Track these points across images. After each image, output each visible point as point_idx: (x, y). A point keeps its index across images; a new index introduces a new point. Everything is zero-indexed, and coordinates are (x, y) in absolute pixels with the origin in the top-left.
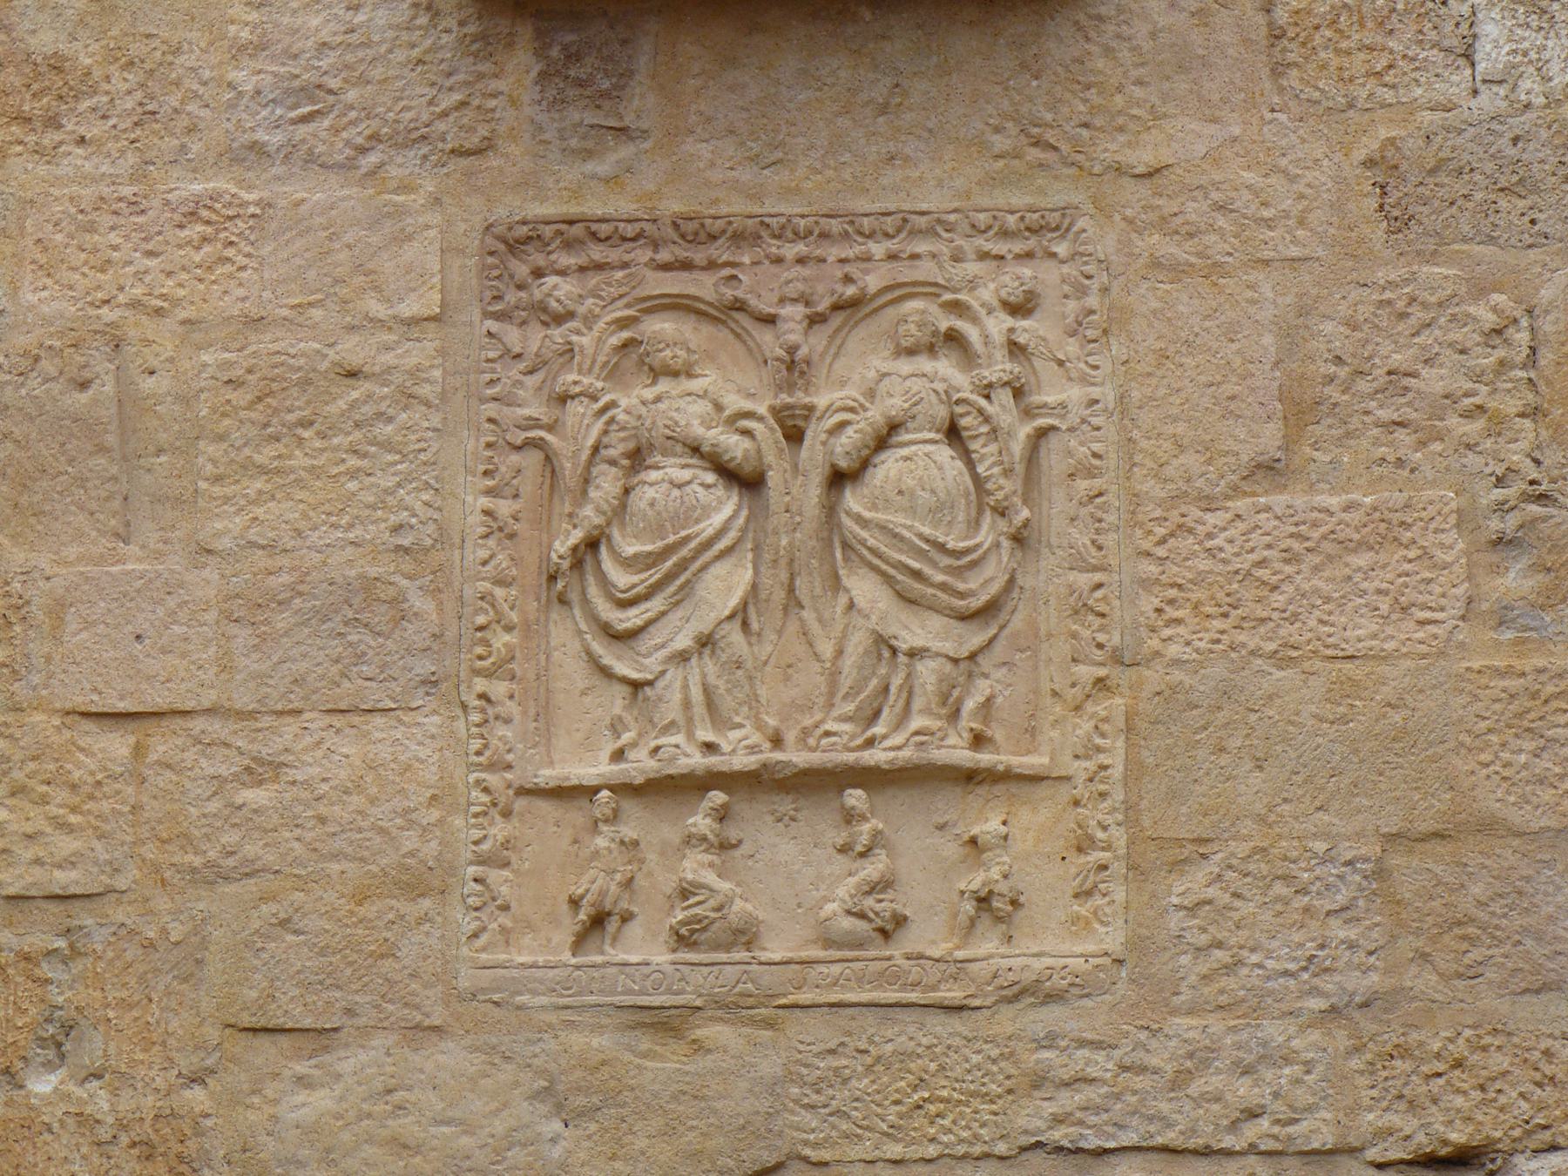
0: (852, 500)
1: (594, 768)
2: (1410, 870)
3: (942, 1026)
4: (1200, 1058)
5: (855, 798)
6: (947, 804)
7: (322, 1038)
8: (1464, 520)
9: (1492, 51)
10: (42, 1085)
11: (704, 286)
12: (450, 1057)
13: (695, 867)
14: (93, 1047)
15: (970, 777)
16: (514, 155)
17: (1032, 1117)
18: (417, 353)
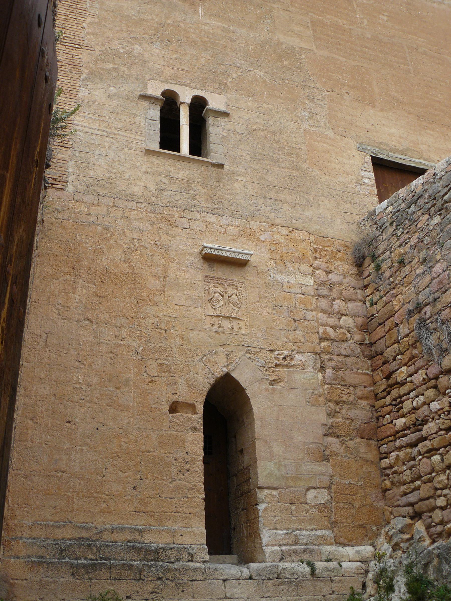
0: (229, 298)
1: (212, 314)
2: (268, 330)
3: (237, 336)
4: (254, 341)
5: (231, 319)
6: (237, 321)
7: (193, 330)
8: (271, 307)
9: (272, 276)
10: (172, 331)
11: (219, 282)
12: (202, 333)
13: (220, 322)
14: (176, 328)
15: (238, 319)
16: (206, 271)
17: (243, 343)
18: (199, 283)
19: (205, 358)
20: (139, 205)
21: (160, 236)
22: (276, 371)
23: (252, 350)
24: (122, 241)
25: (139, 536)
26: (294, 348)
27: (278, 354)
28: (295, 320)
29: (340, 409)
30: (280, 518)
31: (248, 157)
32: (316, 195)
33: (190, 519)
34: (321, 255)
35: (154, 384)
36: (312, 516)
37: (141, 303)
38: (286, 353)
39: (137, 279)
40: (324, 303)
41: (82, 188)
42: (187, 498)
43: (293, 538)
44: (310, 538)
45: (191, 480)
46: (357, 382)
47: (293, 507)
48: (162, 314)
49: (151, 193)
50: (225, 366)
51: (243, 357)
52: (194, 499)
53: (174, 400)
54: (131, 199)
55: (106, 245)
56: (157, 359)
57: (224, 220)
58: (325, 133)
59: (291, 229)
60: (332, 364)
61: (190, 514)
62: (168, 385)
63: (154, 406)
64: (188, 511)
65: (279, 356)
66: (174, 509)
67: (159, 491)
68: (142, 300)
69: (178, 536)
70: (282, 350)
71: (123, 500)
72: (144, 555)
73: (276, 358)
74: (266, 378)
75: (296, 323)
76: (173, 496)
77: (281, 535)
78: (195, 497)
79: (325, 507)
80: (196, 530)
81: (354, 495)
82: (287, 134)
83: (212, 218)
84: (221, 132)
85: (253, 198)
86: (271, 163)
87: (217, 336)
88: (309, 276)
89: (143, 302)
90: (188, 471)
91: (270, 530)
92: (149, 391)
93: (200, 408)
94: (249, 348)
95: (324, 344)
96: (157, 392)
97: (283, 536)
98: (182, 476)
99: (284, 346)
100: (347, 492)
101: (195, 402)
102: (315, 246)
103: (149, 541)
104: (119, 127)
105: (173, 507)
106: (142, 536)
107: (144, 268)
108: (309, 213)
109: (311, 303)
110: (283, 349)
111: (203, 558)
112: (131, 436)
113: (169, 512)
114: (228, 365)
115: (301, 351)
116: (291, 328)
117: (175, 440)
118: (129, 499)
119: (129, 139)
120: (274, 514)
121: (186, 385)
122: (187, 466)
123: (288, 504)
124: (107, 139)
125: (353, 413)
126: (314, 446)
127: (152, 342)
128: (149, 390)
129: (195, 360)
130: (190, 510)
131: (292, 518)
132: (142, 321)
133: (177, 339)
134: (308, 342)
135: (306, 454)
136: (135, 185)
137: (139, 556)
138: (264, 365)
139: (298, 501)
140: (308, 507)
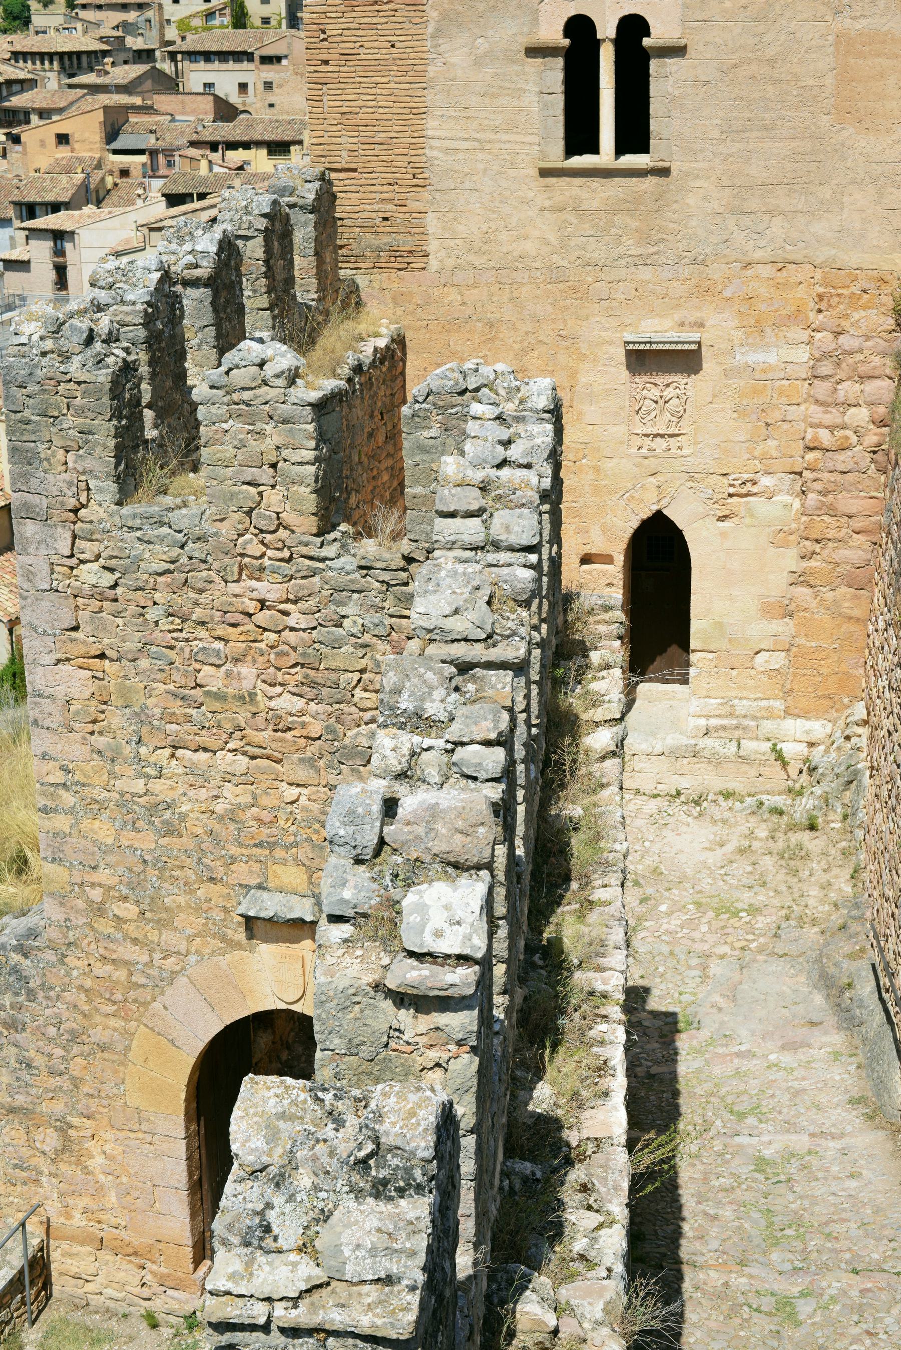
12: (624, 460)
17: (683, 468)
20: (533, 273)
21: (565, 321)
23: (696, 475)
24: (511, 340)
26: (759, 467)
28: (767, 424)
29: (822, 548)
31: (716, 134)
32: (839, 185)
34: (830, 306)
38: (746, 476)
40: (822, 389)
41: (450, 262)
46: (854, 511)
47: (734, 673)
49: (550, 248)
54: (520, 266)
55: (489, 350)
57: (666, 273)
58: (885, 28)
59: (781, 265)
60: (818, 486)
79: (779, 673)
81: (823, 659)
82: (799, 56)
83: (646, 274)
84: (670, 89)
85: (719, 220)
86: (759, 134)
88: (803, 345)
93: (620, 559)
95: (811, 456)
100: (813, 657)
102: (821, 290)
104: (497, 123)
108: (819, 228)
109: (798, 392)
114: (659, 501)
119: (513, 146)
124: (480, 155)
125: (844, 553)
126: (773, 599)
134: (784, 456)
136: (525, 237)
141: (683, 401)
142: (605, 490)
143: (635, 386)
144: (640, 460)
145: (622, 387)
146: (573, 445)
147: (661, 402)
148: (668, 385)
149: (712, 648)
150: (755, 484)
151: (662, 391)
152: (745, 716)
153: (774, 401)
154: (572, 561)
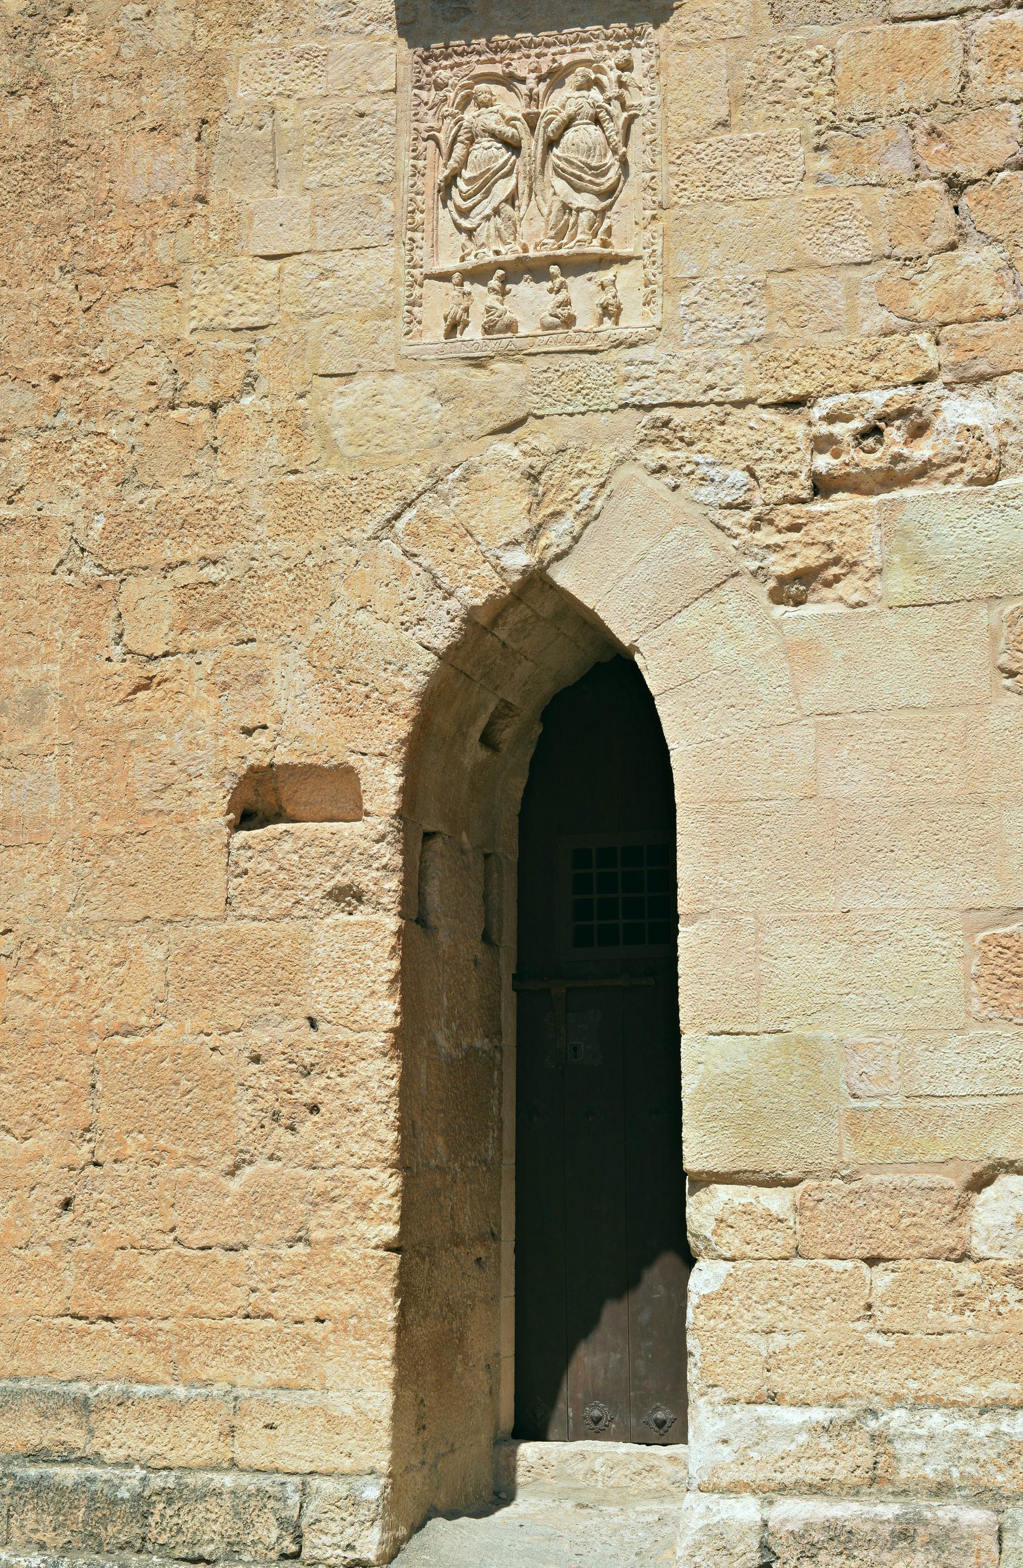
12: (396, 381)
14: (262, 387)
17: (623, 393)
19: (410, 514)
22: (812, 518)
23: (679, 416)
25: (80, 1433)
26: (933, 357)
27: (831, 418)
28: (956, 185)
30: (799, 1338)
33: (318, 1347)
35: (159, 694)
36: (999, 1324)
37: (94, 289)
38: (878, 399)
39: (69, 167)
42: (308, 1242)
43: (862, 1453)
44: (967, 1454)
45: (327, 1154)
47: (882, 1278)
48: (193, 324)
50: (516, 543)
51: (626, 471)
52: (338, 1248)
53: (251, 761)
56: (170, 567)
61: (320, 1320)
62: (225, 686)
63: (158, 804)
64: (307, 1309)
65: (839, 429)
66: (239, 1297)
67: (174, 1217)
68: (99, 272)
69: (251, 1430)
70: (855, 389)
71: (18, 1264)
72: (85, 1523)
73: (822, 444)
74: (754, 565)
75: (964, 201)
76: (242, 1237)
77: (789, 1433)
78: (343, 1238)
80: (341, 1404)
87: (481, 376)
89: (102, 281)
90: (314, 1109)
91: (734, 1401)
92: (132, 735)
94: (662, 413)
96: (170, 735)
97: (803, 1438)
98: (288, 1137)
99: (873, 358)
101: (353, 760)
103: (122, 1453)
105: (240, 1292)
106: (90, 1431)
107: (103, 99)
110: (862, 380)
111: (350, 1547)
112: (54, 962)
113: (222, 1316)
114: (535, 534)
115: (983, 367)
116: (924, 237)
117: (254, 961)
118: (44, 1262)
120: (767, 1319)
121: (310, 677)
122: (309, 1090)
123: (849, 1265)
127: (147, 480)
128: (132, 727)
129: (356, 535)
130: (319, 1304)
131: (873, 1338)
132: (98, 381)
133: (272, 441)
135: (976, 978)
137: (63, 1525)
138: (740, 496)
139: (916, 1242)
140: (976, 1278)
141: (614, 128)
142: (325, 503)
143: (429, 96)
144: (458, 371)
145: (387, 104)
146: (208, 340)
147: (532, 146)
148: (555, 77)
149: (778, 1165)
150: (919, 431)
151: (532, 98)
152: (941, 1490)
153: (977, 90)
154: (198, 802)
